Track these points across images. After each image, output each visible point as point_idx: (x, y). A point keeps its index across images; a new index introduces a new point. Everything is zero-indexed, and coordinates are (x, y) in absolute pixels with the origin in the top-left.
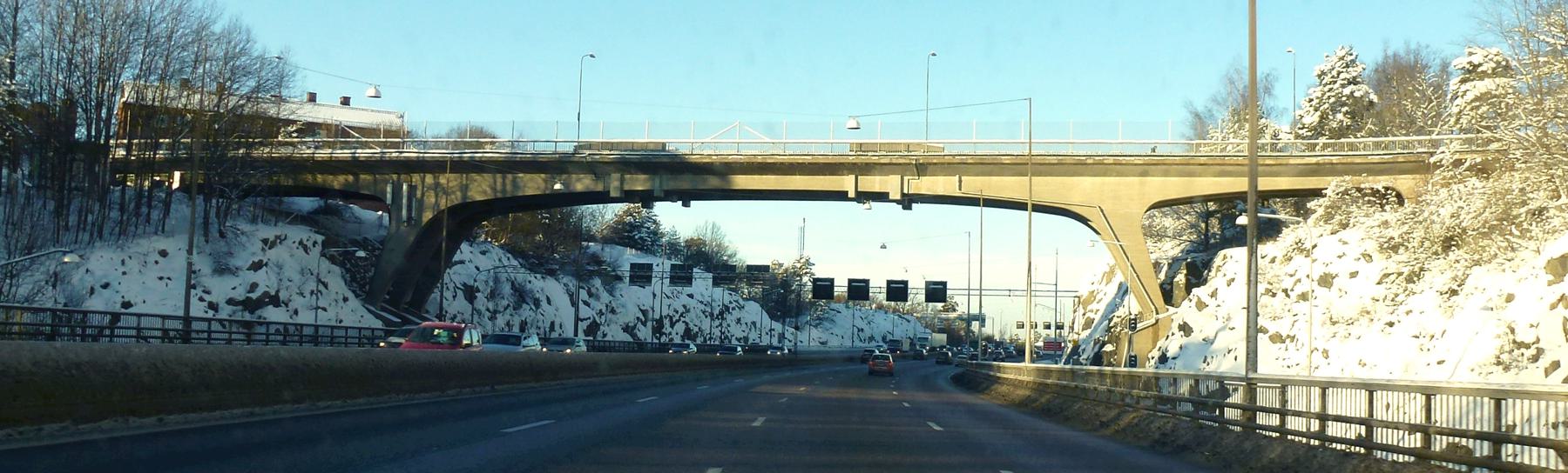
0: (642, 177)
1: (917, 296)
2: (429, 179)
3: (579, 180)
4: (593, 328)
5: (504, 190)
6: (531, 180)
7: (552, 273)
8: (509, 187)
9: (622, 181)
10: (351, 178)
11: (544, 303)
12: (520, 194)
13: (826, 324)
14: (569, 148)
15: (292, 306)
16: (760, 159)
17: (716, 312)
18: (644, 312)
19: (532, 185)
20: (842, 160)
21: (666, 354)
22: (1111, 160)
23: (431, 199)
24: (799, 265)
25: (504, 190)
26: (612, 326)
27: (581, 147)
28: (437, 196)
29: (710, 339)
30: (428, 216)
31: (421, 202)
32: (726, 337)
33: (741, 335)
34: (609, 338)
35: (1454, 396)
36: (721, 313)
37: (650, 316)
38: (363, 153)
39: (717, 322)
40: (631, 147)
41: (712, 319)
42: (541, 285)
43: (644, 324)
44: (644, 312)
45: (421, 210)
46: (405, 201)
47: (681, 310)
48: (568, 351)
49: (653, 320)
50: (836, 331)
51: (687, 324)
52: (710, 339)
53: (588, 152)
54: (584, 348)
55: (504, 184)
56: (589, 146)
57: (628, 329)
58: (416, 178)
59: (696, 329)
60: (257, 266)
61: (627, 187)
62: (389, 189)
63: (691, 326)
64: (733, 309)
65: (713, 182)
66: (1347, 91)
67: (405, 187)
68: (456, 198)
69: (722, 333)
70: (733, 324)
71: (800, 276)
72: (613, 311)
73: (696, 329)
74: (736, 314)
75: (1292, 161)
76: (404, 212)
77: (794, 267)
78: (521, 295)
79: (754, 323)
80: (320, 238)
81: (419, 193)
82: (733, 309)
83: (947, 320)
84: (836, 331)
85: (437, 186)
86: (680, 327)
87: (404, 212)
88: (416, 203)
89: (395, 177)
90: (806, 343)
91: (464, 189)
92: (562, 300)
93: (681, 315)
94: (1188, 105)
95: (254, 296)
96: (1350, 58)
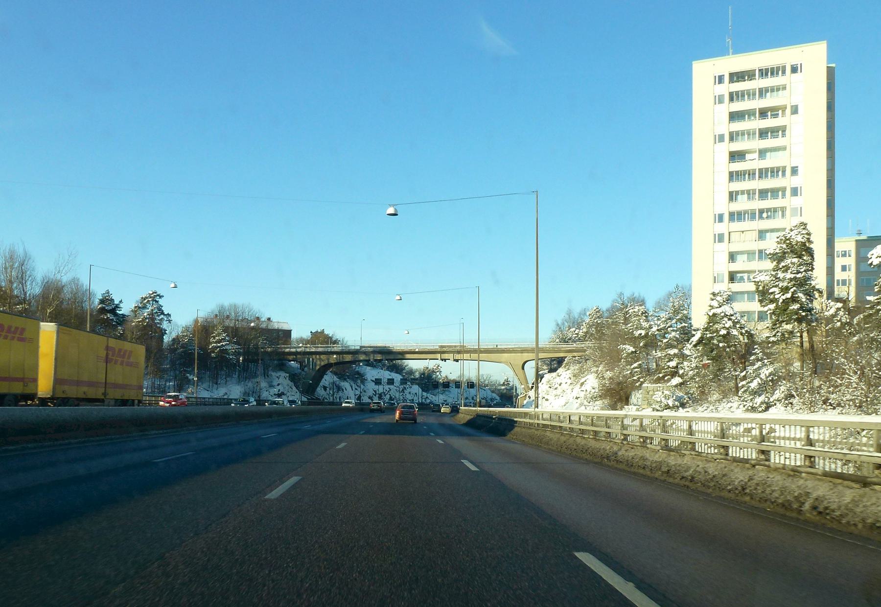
0: (379, 355)
1: (464, 385)
2: (318, 356)
3: (361, 356)
4: (359, 398)
5: (340, 360)
6: (347, 356)
7: (345, 379)
8: (341, 359)
9: (374, 356)
10: (295, 357)
11: (345, 390)
12: (344, 361)
13: (447, 393)
14: (359, 348)
15: (287, 395)
16: (413, 350)
17: (401, 390)
18: (375, 391)
19: (348, 358)
20: (437, 350)
21: (264, 407)
22: (511, 349)
23: (318, 363)
24: (435, 368)
25: (340, 360)
26: (365, 396)
27: (361, 347)
28: (320, 361)
29: (399, 400)
30: (318, 367)
31: (316, 363)
32: (405, 400)
33: (411, 398)
34: (364, 401)
35: (748, 423)
36: (403, 390)
37: (378, 392)
38: (299, 350)
39: (402, 394)
40: (376, 347)
41: (400, 393)
42: (345, 385)
43: (375, 395)
44: (375, 391)
45: (316, 366)
46: (311, 363)
47: (388, 390)
48: (294, 406)
49: (379, 394)
50: (451, 396)
51: (390, 395)
52: (399, 400)
53: (364, 349)
54: (255, 403)
55: (340, 358)
56: (364, 347)
57: (370, 398)
58: (314, 356)
59: (394, 397)
60: (278, 385)
61: (375, 358)
62: (306, 360)
63: (392, 396)
64: (408, 388)
65: (400, 357)
66: (595, 321)
67: (311, 359)
68: (326, 362)
69: (404, 398)
70: (408, 394)
71: (436, 372)
72: (365, 392)
73: (394, 397)
74: (408, 390)
75: (562, 349)
76: (311, 366)
77: (433, 369)
78: (339, 389)
79: (416, 394)
80: (288, 375)
81: (315, 361)
82: (408, 388)
83: (501, 389)
84: (451, 396)
85: (320, 359)
86: (388, 396)
87: (311, 366)
88: (315, 365)
89: (308, 356)
90: (437, 401)
91: (328, 359)
92: (349, 388)
93: (388, 392)
94: (556, 321)
95: (280, 393)
96: (598, 310)
